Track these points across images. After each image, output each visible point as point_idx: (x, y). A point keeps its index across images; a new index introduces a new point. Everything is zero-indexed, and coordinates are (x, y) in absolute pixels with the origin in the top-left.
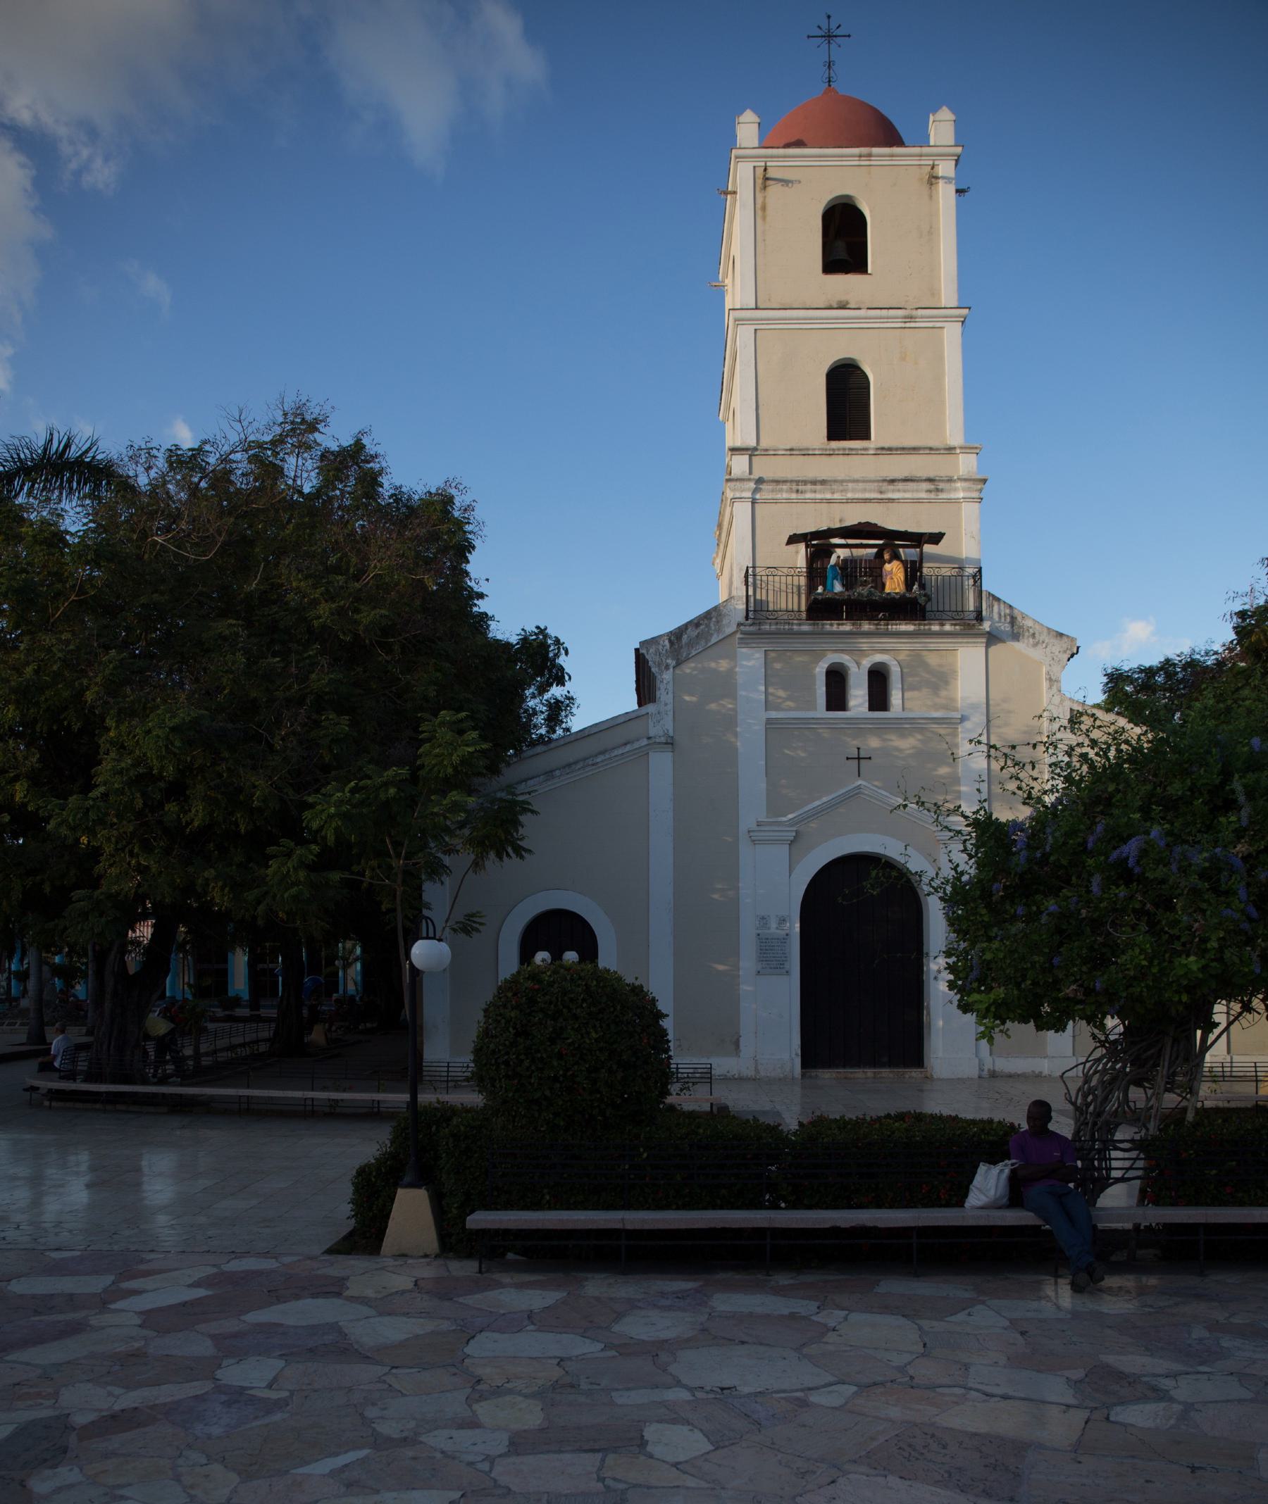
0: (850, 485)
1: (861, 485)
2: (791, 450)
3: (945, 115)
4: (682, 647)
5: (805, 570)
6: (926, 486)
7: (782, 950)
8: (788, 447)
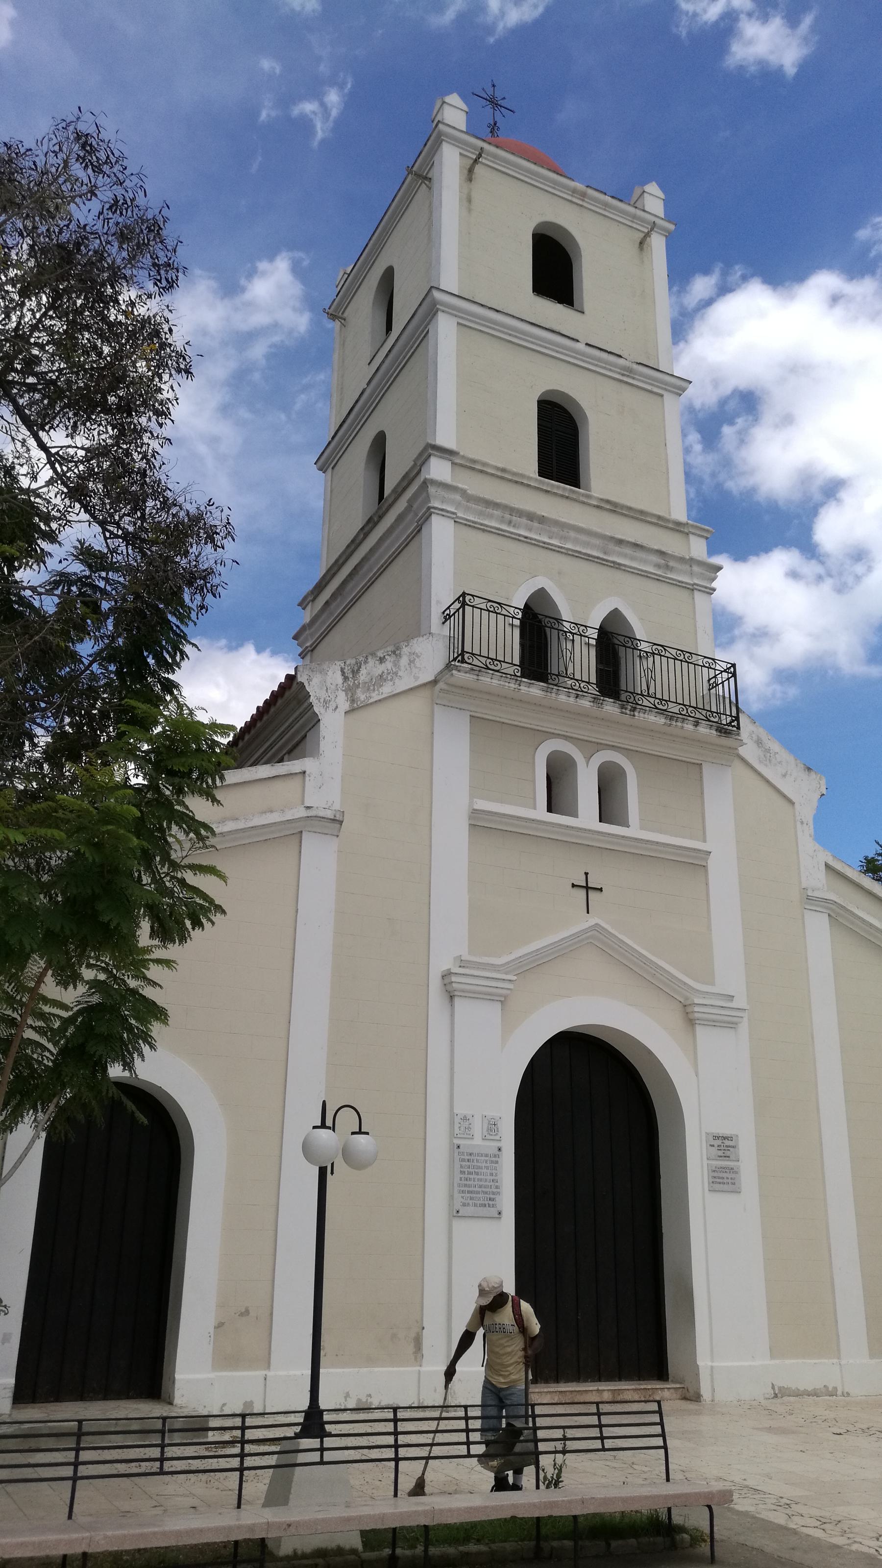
0: (572, 534)
1: (583, 538)
2: (504, 470)
3: (653, 188)
4: (358, 686)
5: (30, 961)
6: (655, 558)
7: (492, 1174)
8: (500, 465)
